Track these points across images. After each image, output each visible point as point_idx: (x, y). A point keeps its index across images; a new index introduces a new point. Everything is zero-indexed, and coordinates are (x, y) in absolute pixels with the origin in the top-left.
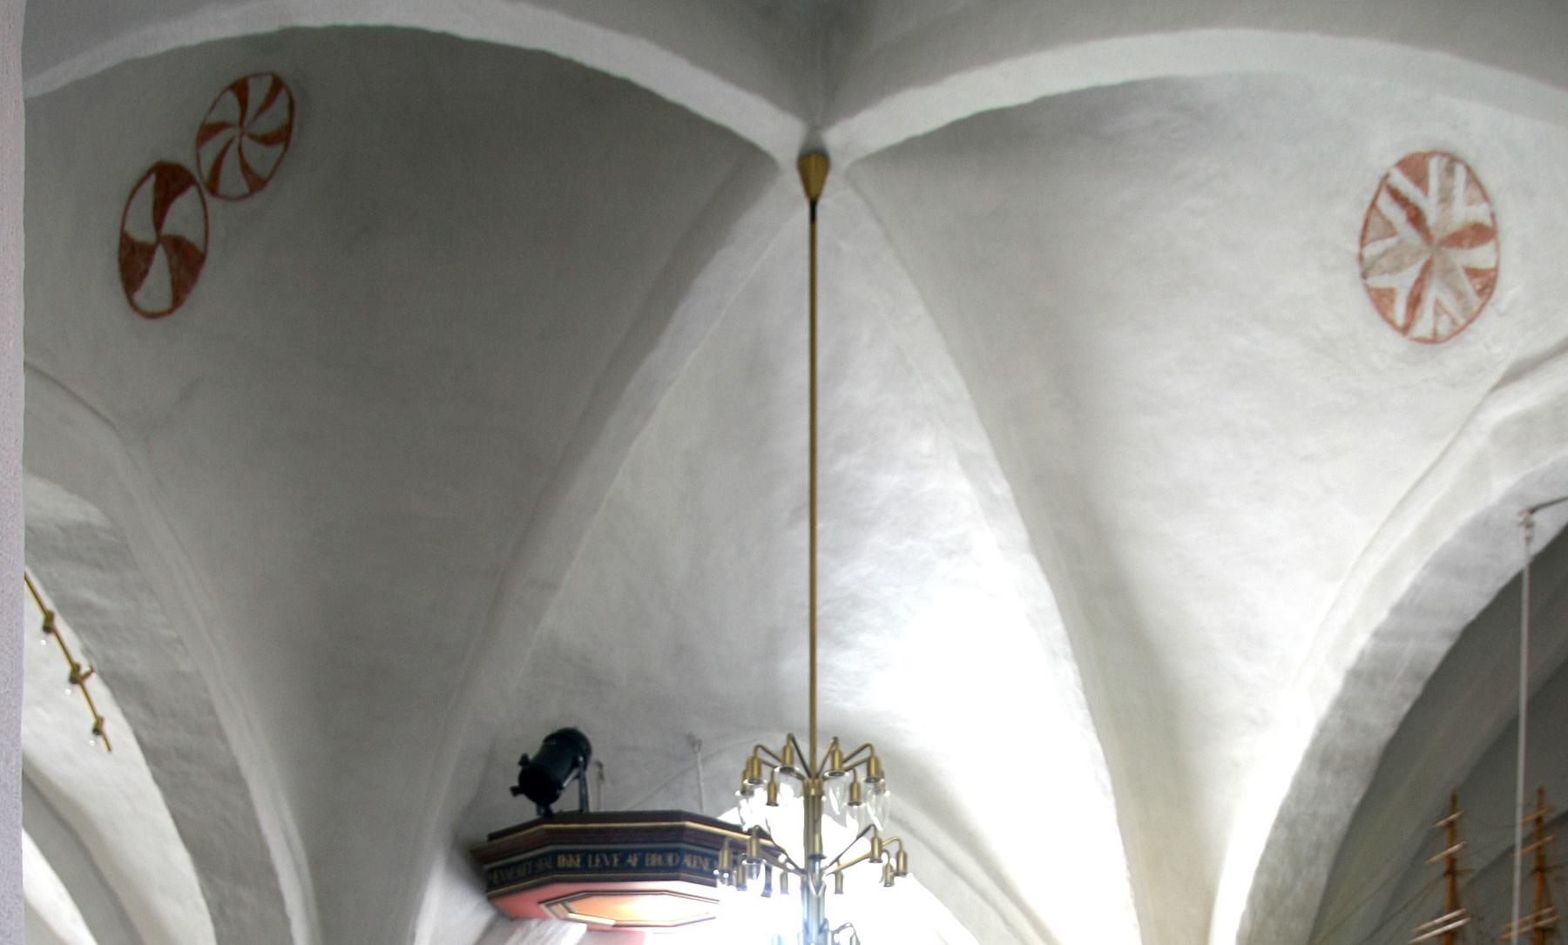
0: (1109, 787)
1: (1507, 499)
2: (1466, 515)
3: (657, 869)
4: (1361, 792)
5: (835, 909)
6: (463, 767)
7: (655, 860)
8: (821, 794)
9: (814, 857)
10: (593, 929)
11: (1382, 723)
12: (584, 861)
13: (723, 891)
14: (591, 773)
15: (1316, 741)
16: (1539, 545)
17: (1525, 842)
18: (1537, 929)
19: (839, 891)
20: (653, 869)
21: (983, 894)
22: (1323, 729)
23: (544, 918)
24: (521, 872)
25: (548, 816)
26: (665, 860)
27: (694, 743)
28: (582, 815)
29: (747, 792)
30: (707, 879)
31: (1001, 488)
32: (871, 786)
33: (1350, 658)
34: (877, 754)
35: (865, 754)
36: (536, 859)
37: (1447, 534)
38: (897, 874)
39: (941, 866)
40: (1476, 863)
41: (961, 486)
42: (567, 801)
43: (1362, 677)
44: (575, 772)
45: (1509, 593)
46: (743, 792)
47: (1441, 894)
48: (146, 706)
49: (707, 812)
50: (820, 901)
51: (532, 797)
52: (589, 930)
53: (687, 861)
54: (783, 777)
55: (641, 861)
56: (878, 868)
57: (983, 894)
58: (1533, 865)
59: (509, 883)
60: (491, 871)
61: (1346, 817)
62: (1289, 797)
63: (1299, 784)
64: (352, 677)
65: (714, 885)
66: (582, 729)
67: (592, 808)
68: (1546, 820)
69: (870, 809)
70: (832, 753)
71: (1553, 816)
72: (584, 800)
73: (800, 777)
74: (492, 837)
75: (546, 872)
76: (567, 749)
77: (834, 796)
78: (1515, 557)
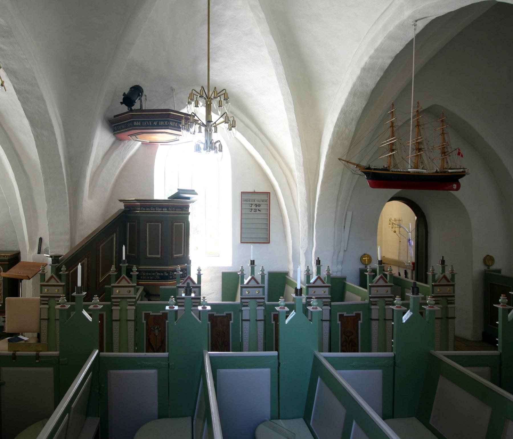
0: (292, 102)
1: (409, 18)
2: (397, 22)
3: (162, 126)
4: (365, 104)
5: (215, 137)
6: (107, 98)
7: (162, 123)
8: (211, 103)
9: (209, 121)
10: (143, 143)
11: (371, 83)
12: (141, 123)
13: (184, 132)
14: (143, 98)
15: (352, 89)
16: (418, 31)
17: (413, 117)
18: (417, 143)
19: (216, 132)
20: (161, 126)
21: (255, 133)
22: (354, 85)
23: (130, 140)
24: (123, 127)
25: (131, 110)
26: (164, 123)
27: (172, 90)
28: (141, 110)
29: (189, 103)
30: (178, 129)
31: (262, 15)
32: (225, 101)
33: (362, 64)
34: (227, 92)
35: (224, 92)
36: (127, 123)
37: (391, 28)
38: (233, 127)
39: (243, 125)
40: (400, 123)
41: (251, 14)
42: (136, 106)
43: (366, 70)
44: (139, 98)
45: (409, 45)
46: (189, 103)
47: (389, 132)
48: (16, 78)
49: (176, 109)
50: (210, 135)
51: (126, 105)
52: (142, 143)
53: (171, 124)
54: (200, 99)
55: (158, 123)
56: (227, 125)
57: (255, 133)
58: (416, 124)
59: (120, 130)
60: (115, 126)
61: (361, 111)
62: (344, 105)
63: (347, 101)
64: (77, 71)
65: (180, 131)
66: (140, 85)
67: (143, 108)
68: (419, 111)
69: (226, 108)
70: (214, 92)
71: (421, 110)
72: (141, 106)
73: (205, 99)
74: (115, 116)
75: (131, 126)
76: (136, 91)
77: (214, 104)
78: (411, 35)
